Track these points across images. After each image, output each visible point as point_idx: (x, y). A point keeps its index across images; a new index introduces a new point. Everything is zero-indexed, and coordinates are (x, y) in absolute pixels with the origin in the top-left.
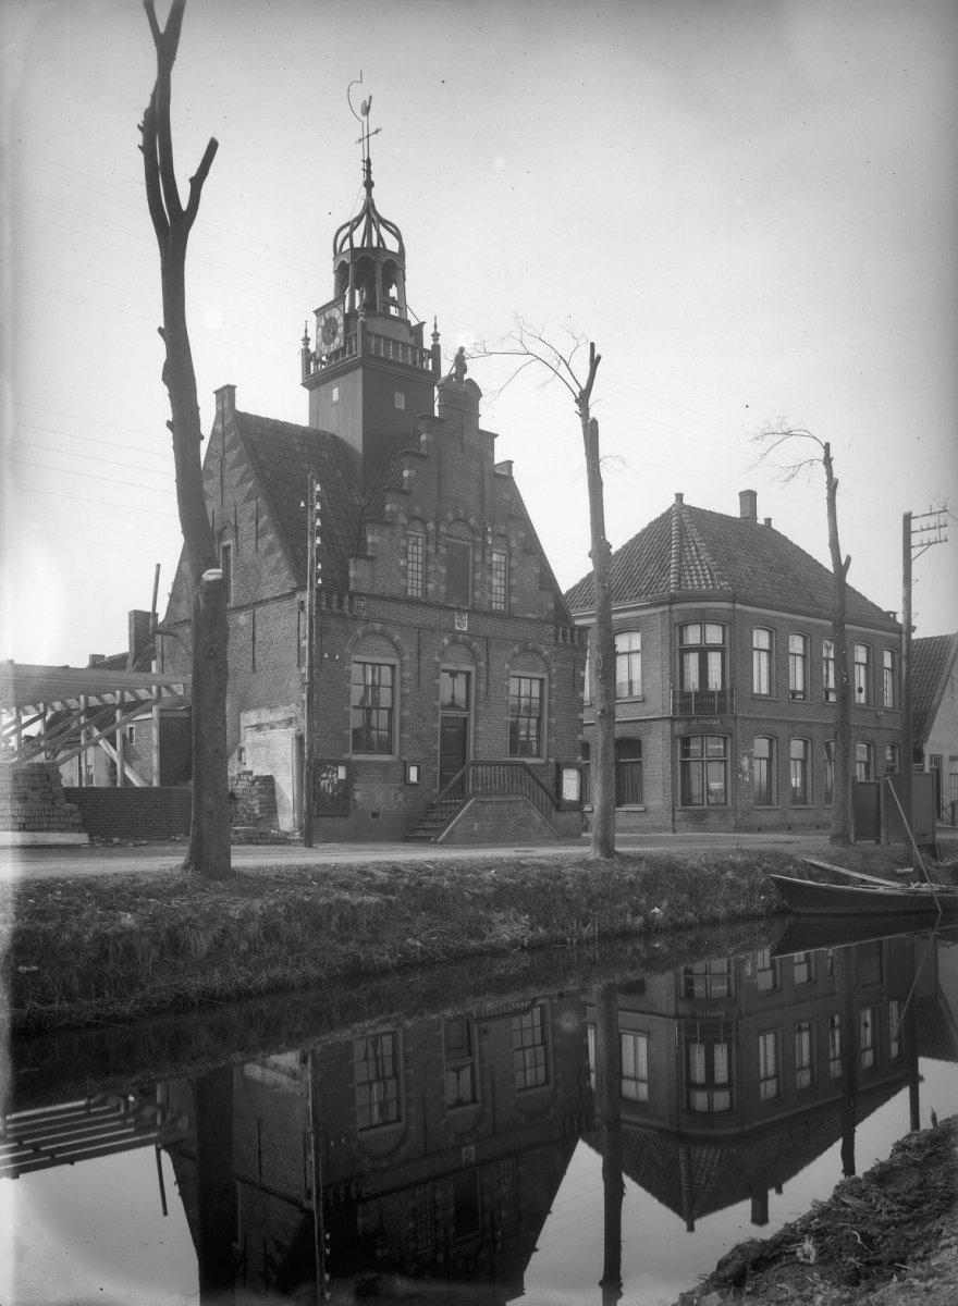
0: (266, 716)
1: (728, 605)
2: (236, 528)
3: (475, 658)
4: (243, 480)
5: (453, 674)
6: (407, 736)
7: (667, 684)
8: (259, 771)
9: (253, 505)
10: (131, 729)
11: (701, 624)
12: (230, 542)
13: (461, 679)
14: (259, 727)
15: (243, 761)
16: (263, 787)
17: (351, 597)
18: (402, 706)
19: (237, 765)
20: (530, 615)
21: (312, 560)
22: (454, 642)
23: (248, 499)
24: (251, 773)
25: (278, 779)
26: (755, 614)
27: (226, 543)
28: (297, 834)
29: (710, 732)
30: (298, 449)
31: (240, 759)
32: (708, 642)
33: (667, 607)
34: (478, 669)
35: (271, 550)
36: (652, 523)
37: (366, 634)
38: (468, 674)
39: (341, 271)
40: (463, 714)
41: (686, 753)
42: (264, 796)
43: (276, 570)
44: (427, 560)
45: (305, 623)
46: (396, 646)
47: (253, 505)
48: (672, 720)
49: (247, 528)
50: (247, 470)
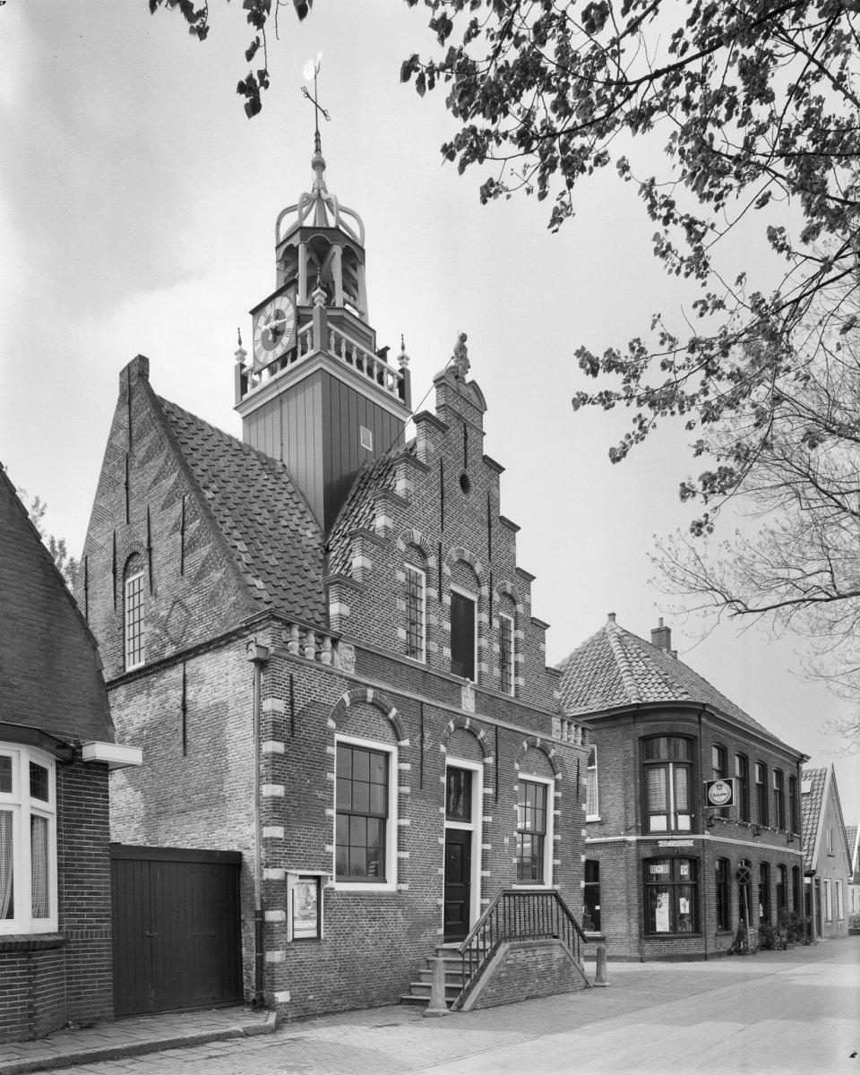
2: (150, 550)
39: (288, 255)
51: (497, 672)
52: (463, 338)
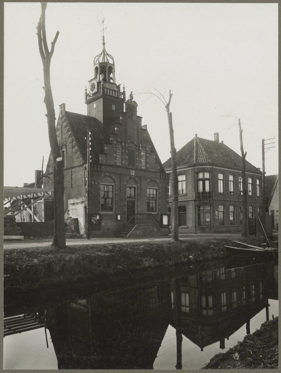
0: (75, 201)
1: (211, 167)
3: (137, 183)
4: (68, 131)
5: (130, 188)
6: (117, 206)
7: (193, 190)
8: (74, 217)
9: (71, 138)
10: (36, 205)
11: (203, 172)
12: (64, 149)
13: (133, 189)
14: (73, 204)
15: (69, 214)
16: (75, 222)
17: (100, 165)
18: (116, 198)
19: (67, 215)
20: (153, 170)
21: (89, 155)
22: (130, 178)
23: (69, 137)
24: (71, 217)
25: (79, 219)
26: (219, 169)
27: (63, 150)
28: (85, 235)
29: (206, 204)
30: (84, 122)
31: (68, 213)
32: (205, 177)
33: (193, 168)
34: (137, 186)
35: (76, 152)
36: (188, 143)
37: (105, 176)
38: (135, 188)
40: (133, 200)
41: (199, 210)
42: (75, 224)
43: (78, 158)
44: (122, 154)
45: (87, 173)
46: (113, 179)
47: (71, 138)
48: (195, 201)
49: (69, 145)
50: (69, 129)
51: (123, 157)
52: (132, 92)
